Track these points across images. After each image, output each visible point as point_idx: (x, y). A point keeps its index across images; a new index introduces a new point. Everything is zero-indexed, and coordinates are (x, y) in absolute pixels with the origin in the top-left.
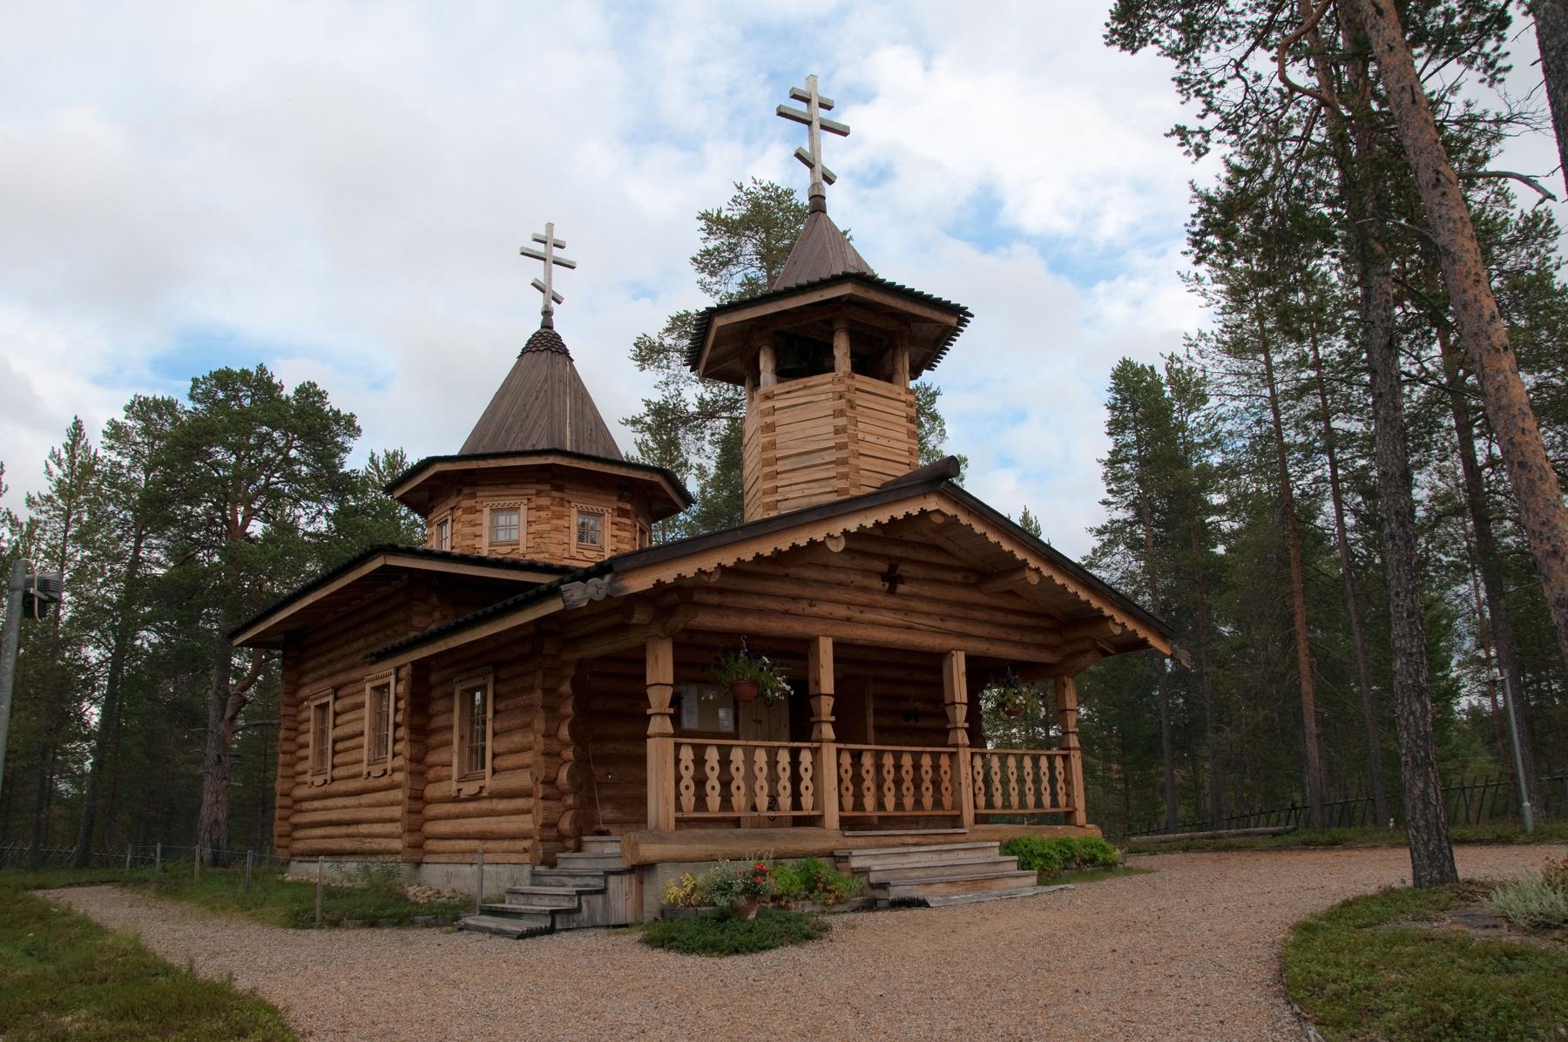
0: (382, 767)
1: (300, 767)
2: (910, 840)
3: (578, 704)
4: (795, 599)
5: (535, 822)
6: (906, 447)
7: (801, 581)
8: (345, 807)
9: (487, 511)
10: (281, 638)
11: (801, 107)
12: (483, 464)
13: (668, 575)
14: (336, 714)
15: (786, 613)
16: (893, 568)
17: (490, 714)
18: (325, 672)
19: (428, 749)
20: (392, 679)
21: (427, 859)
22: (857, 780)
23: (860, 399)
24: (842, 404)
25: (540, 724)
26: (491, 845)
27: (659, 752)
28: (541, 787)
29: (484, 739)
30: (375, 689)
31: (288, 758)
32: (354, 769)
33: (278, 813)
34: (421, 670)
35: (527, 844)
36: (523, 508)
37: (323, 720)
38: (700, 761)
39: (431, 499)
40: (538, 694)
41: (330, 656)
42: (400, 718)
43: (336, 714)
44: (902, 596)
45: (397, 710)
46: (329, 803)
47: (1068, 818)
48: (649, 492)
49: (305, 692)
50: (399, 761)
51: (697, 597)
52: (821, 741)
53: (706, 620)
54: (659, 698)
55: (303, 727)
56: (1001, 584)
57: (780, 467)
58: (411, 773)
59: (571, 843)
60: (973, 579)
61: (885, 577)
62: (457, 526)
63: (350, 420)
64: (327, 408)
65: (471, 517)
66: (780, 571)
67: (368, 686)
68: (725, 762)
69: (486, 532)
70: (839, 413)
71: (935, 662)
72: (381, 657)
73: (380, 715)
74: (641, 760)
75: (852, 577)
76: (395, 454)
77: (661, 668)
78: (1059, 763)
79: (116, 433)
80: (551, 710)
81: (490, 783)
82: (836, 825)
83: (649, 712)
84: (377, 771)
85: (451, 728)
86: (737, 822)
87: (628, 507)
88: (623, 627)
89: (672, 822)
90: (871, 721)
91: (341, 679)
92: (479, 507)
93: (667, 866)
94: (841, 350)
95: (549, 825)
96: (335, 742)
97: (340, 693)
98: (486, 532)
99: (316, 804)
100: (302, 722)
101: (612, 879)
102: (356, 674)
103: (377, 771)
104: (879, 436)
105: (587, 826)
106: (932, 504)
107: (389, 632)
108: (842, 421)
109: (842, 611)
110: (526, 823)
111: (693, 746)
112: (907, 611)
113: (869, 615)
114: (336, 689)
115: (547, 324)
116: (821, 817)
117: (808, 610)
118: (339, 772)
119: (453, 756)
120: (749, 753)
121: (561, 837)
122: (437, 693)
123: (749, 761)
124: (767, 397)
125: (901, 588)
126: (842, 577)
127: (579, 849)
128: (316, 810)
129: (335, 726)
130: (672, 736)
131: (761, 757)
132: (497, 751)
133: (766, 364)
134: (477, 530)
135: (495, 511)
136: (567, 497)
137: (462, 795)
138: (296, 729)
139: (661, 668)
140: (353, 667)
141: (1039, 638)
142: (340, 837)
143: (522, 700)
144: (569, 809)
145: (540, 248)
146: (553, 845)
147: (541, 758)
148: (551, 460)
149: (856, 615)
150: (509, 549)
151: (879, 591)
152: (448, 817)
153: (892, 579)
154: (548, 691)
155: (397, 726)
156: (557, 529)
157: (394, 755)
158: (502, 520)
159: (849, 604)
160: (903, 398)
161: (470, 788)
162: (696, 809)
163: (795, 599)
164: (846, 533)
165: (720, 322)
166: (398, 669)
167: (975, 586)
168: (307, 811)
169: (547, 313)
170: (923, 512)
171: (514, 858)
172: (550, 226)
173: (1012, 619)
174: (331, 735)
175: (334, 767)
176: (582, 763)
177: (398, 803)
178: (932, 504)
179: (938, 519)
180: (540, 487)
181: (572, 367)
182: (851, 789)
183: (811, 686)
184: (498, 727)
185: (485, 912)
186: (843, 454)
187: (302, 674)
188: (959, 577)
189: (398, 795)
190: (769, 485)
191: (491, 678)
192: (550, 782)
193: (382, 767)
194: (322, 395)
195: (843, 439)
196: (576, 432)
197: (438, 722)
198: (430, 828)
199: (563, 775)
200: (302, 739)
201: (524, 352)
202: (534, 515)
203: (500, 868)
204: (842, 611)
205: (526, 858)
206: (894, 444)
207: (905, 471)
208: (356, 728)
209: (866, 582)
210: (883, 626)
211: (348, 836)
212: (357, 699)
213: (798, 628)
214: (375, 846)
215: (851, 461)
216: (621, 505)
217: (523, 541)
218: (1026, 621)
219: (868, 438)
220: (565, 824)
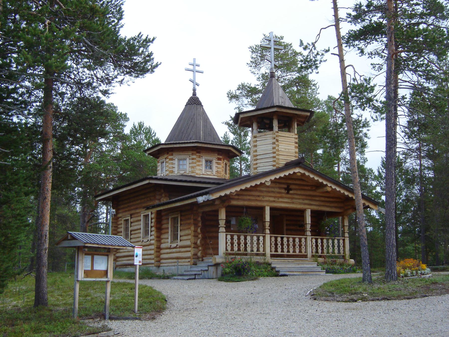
2: (290, 261)
3: (202, 223)
4: (259, 196)
5: (191, 254)
9: (176, 160)
14: (131, 223)
15: (256, 200)
16: (288, 186)
17: (179, 225)
18: (127, 209)
19: (161, 234)
22: (276, 244)
23: (280, 139)
24: (274, 141)
25: (193, 228)
26: (180, 260)
29: (178, 231)
34: (159, 213)
35: (189, 260)
36: (188, 159)
40: (192, 220)
41: (129, 204)
42: (153, 224)
43: (131, 223)
44: (291, 194)
45: (151, 222)
48: (228, 153)
50: (153, 237)
53: (234, 203)
54: (222, 223)
55: (120, 226)
56: (321, 190)
57: (258, 157)
58: (157, 241)
59: (201, 259)
61: (285, 189)
62: (167, 164)
63: (125, 115)
64: (118, 112)
65: (172, 161)
67: (142, 215)
69: (176, 166)
70: (274, 143)
71: (302, 212)
72: (148, 208)
73: (146, 225)
74: (217, 238)
76: (141, 122)
77: (222, 215)
78: (341, 241)
80: (196, 225)
81: (180, 244)
82: (269, 256)
84: (145, 240)
85: (168, 228)
87: (221, 157)
90: (285, 228)
91: (133, 212)
94: (275, 124)
95: (195, 254)
96: (131, 231)
97: (133, 216)
101: (209, 267)
102: (137, 211)
103: (145, 240)
105: (205, 254)
107: (148, 199)
108: (274, 146)
109: (272, 199)
110: (189, 254)
112: (292, 198)
113: (280, 200)
114: (131, 215)
115: (194, 94)
117: (263, 199)
120: (328, 240)
121: (198, 258)
122: (164, 218)
125: (291, 192)
127: (203, 260)
129: (131, 226)
131: (255, 238)
132: (181, 235)
136: (201, 155)
138: (116, 227)
139: (222, 215)
140: (137, 209)
143: (188, 221)
144: (200, 250)
145: (191, 67)
146: (196, 260)
147: (193, 238)
150: (183, 172)
151: (283, 193)
152: (167, 253)
153: (288, 190)
154: (195, 220)
155: (151, 227)
156: (198, 165)
157: (151, 236)
158: (181, 162)
159: (275, 197)
161: (174, 245)
163: (259, 196)
165: (241, 116)
167: (315, 190)
168: (121, 252)
169: (194, 90)
170: (294, 173)
171: (186, 264)
172: (194, 60)
173: (326, 199)
175: (131, 239)
176: (204, 238)
177: (153, 250)
178: (297, 170)
179: (299, 174)
181: (203, 108)
182: (274, 246)
184: (181, 228)
185: (178, 275)
186: (274, 155)
188: (309, 188)
189: (153, 247)
190: (255, 162)
192: (195, 243)
193: (148, 239)
195: (274, 150)
196: (204, 133)
197: (164, 226)
198: (162, 256)
199: (199, 242)
202: (191, 161)
203: (182, 267)
204: (272, 199)
205: (189, 264)
206: (290, 151)
208: (138, 227)
209: (280, 191)
210: (284, 203)
212: (139, 218)
213: (259, 204)
215: (277, 157)
218: (331, 200)
219: (282, 150)
220: (199, 254)
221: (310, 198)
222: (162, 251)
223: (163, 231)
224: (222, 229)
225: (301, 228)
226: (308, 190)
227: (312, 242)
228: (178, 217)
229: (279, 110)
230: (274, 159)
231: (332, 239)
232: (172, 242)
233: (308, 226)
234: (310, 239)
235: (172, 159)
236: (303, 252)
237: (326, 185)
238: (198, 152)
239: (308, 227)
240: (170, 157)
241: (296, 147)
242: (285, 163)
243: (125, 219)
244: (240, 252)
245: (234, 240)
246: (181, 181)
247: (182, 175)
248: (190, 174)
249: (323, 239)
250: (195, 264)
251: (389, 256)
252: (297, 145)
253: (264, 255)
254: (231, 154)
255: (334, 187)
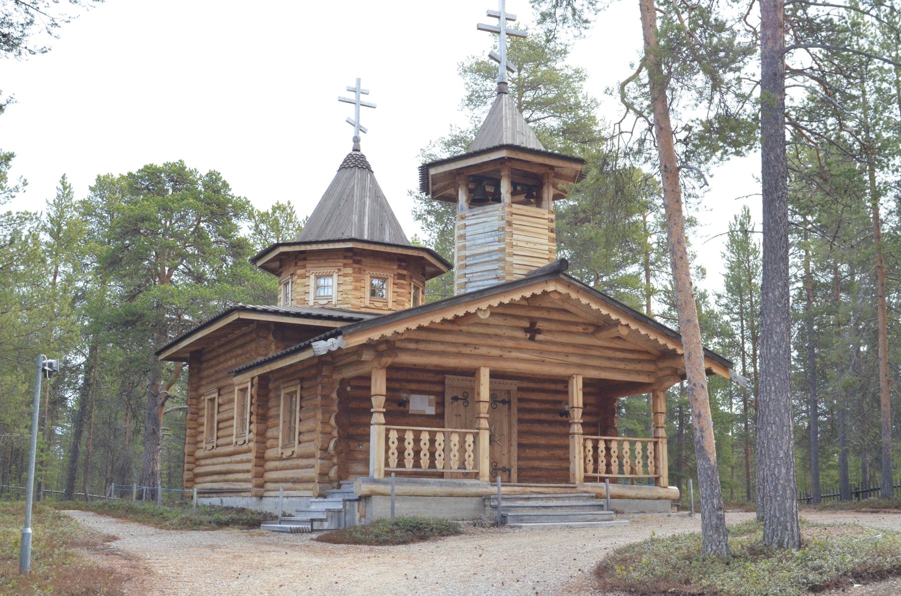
0: (243, 439)
1: (199, 438)
4: (465, 345)
6: (547, 248)
7: (470, 334)
8: (223, 463)
9: (312, 277)
10: (188, 355)
11: (494, 22)
12: (308, 248)
13: (388, 332)
16: (533, 324)
20: (249, 385)
21: (266, 494)
23: (515, 220)
25: (319, 416)
26: (297, 486)
27: (377, 432)
28: (319, 452)
30: (241, 390)
31: (192, 431)
32: (228, 440)
33: (186, 466)
36: (335, 276)
37: (213, 409)
38: (401, 440)
39: (281, 267)
40: (319, 398)
43: (219, 405)
44: (541, 342)
46: (215, 460)
47: (656, 481)
48: (417, 265)
49: (202, 390)
51: (398, 344)
52: (479, 429)
53: (405, 359)
54: (378, 403)
59: (335, 484)
60: (591, 329)
61: (526, 330)
62: (295, 286)
65: (303, 280)
66: (456, 328)
68: (432, 441)
69: (312, 290)
71: (565, 381)
74: (366, 438)
75: (505, 331)
77: (379, 385)
79: (87, 208)
81: (297, 449)
83: (372, 410)
86: (441, 475)
87: (405, 272)
88: (360, 363)
89: (583, 477)
91: (222, 384)
92: (307, 274)
93: (378, 497)
94: (505, 188)
95: (323, 474)
96: (218, 423)
97: (222, 392)
98: (312, 290)
99: (208, 461)
100: (200, 410)
104: (527, 242)
106: (551, 288)
109: (496, 352)
111: (398, 430)
112: (541, 352)
113: (515, 354)
115: (356, 149)
116: (478, 473)
118: (221, 441)
119: (278, 432)
121: (331, 481)
123: (447, 440)
124: (463, 218)
125: (539, 337)
126: (498, 331)
127: (339, 486)
128: (208, 465)
129: (219, 412)
130: (384, 424)
131: (455, 439)
133: (462, 197)
134: (306, 289)
135: (318, 277)
137: (284, 456)
139: (379, 385)
141: (639, 367)
142: (221, 481)
145: (352, 96)
147: (320, 435)
148: (350, 245)
149: (506, 354)
150: (326, 301)
152: (276, 469)
153: (532, 331)
154: (324, 397)
158: (322, 282)
159: (502, 348)
160: (546, 217)
161: (288, 452)
162: (414, 466)
163: (465, 345)
164: (490, 307)
166: (253, 379)
167: (593, 334)
169: (356, 140)
170: (545, 293)
172: (359, 81)
174: (216, 418)
175: (218, 438)
180: (346, 261)
183: (476, 396)
187: (201, 379)
188: (580, 329)
191: (299, 386)
192: (324, 449)
193: (243, 439)
194: (226, 185)
197: (272, 412)
200: (200, 420)
201: (342, 168)
203: (301, 499)
204: (496, 352)
207: (546, 263)
208: (230, 415)
210: (525, 360)
211: (225, 481)
213: (466, 363)
214: (238, 487)
216: (400, 271)
217: (334, 296)
218: (630, 356)
219: (520, 244)
220: (333, 473)
221: (581, 351)
222: (270, 465)
223: (271, 422)
224: (378, 418)
225: (564, 418)
226: (578, 333)
227: (585, 448)
228: (296, 392)
229: (513, 155)
230: (501, 264)
231: (606, 441)
232: (285, 447)
233: (575, 413)
234: (582, 441)
235: (304, 276)
236: (469, 468)
237: (617, 323)
238: (358, 262)
239: (577, 415)
240: (300, 272)
241: (551, 240)
242: (525, 272)
243: (209, 397)
244: (419, 470)
245: (422, 443)
246: (319, 317)
247: (323, 307)
248: (338, 307)
249: (611, 441)
250: (322, 495)
251: (776, 487)
252: (553, 235)
253: (476, 476)
254: (429, 269)
255: (633, 327)
